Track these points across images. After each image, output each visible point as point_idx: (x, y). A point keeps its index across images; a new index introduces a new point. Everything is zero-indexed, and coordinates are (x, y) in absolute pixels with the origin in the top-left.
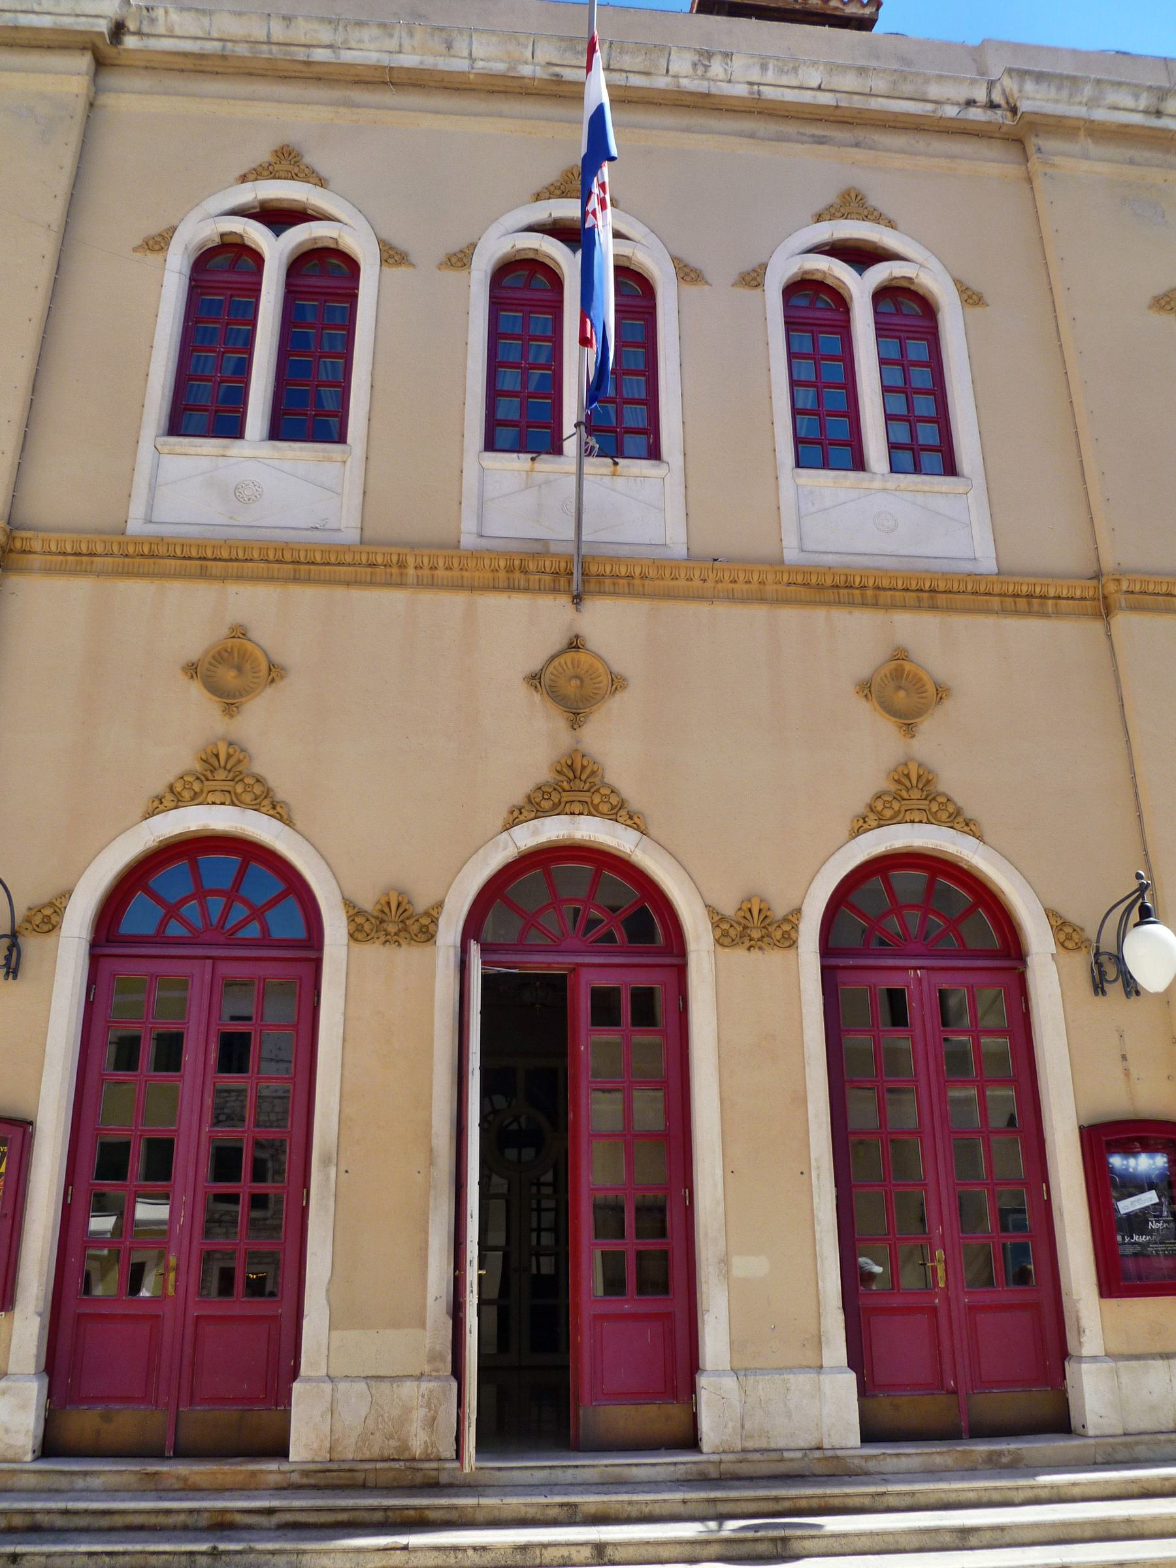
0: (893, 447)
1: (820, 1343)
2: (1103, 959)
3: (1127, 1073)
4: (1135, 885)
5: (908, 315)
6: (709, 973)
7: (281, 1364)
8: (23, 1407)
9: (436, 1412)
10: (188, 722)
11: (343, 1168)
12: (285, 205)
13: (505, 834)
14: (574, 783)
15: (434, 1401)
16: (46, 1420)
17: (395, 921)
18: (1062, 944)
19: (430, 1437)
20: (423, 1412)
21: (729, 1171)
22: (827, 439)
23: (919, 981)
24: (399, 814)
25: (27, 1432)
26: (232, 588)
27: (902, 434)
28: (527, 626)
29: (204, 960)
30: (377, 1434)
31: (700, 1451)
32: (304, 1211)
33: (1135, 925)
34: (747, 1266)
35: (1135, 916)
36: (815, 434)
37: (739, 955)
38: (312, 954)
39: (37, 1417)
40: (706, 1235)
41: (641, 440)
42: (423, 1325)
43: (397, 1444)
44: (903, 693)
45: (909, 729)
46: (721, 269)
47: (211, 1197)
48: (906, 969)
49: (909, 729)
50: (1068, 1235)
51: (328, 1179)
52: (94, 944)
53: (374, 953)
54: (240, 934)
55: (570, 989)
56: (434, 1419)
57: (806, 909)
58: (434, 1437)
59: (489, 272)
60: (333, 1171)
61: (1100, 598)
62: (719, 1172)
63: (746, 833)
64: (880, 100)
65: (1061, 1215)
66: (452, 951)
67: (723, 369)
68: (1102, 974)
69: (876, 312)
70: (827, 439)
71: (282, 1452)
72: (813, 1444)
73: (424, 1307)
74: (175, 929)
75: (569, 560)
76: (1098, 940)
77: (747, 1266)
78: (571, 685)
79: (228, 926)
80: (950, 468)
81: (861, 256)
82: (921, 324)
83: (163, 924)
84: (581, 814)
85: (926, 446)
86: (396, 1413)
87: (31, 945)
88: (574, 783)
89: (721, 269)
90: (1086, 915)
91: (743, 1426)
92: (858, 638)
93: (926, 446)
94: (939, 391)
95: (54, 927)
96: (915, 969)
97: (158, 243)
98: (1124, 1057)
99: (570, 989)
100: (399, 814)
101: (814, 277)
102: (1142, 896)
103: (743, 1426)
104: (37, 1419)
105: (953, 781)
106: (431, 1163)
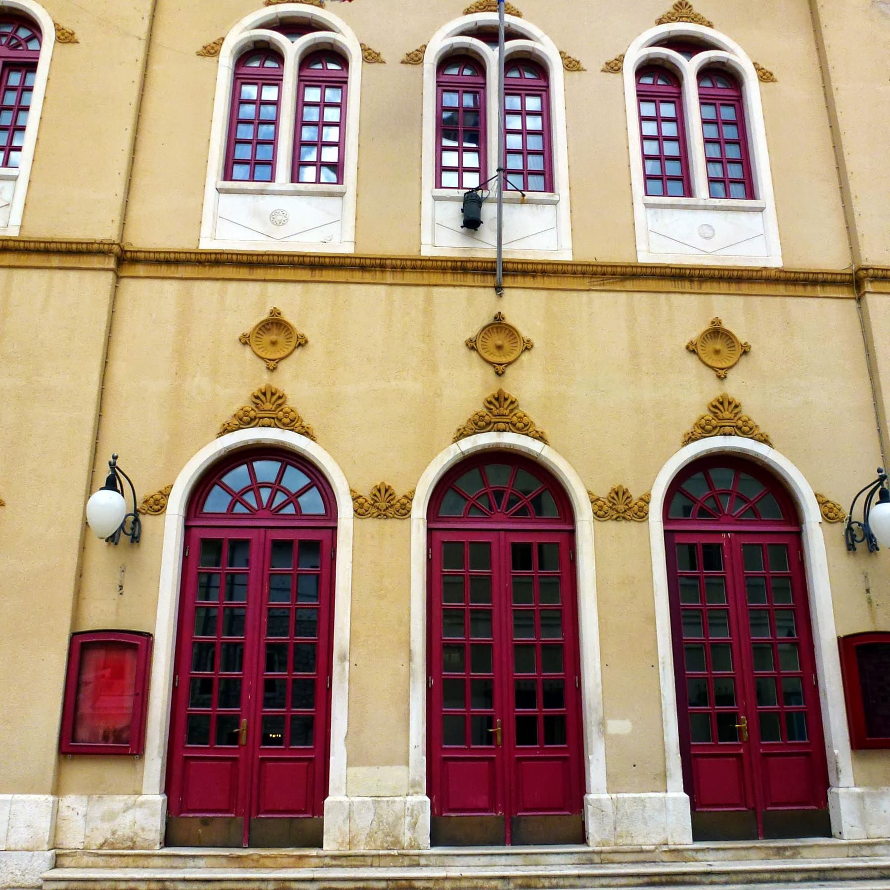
0: (712, 180)
1: (665, 776)
2: (854, 526)
3: (870, 602)
4: (876, 476)
5: (723, 80)
6: (592, 542)
7: (320, 787)
8: (153, 815)
9: (417, 819)
10: (243, 378)
11: (354, 661)
12: (296, 21)
13: (455, 444)
14: (500, 410)
15: (416, 812)
16: (166, 824)
17: (383, 504)
18: (826, 515)
19: (413, 835)
20: (408, 819)
21: (605, 665)
22: (669, 176)
23: (729, 541)
24: (382, 417)
25: (156, 831)
26: (271, 286)
27: (717, 171)
28: (465, 308)
29: (258, 559)
30: (380, 833)
31: (588, 846)
32: (329, 690)
33: (877, 503)
34: (619, 727)
35: (876, 497)
36: (658, 172)
37: (611, 526)
38: (331, 524)
39: (162, 821)
40: (590, 706)
41: (540, 180)
42: (408, 764)
43: (392, 839)
44: (718, 346)
45: (722, 378)
46: (593, 62)
47: (269, 545)
48: (721, 532)
49: (722, 378)
50: (830, 708)
51: (344, 669)
52: (187, 518)
53: (371, 525)
54: (281, 512)
55: (502, 524)
56: (416, 823)
57: (653, 493)
58: (415, 835)
59: (436, 64)
60: (347, 664)
61: (855, 282)
62: (598, 665)
63: (614, 422)
64: (626, 860)
65: (825, 694)
66: (421, 522)
67: (597, 120)
68: (853, 537)
69: (699, 87)
70: (669, 176)
71: (320, 846)
72: (662, 841)
73: (408, 752)
74: (239, 509)
75: (494, 262)
76: (851, 513)
77: (619, 727)
78: (498, 342)
79: (274, 506)
80: (751, 194)
81: (689, 45)
82: (731, 94)
83: (232, 506)
84: (504, 431)
85: (736, 177)
86: (391, 819)
87: (147, 521)
88: (500, 410)
89: (593, 62)
90: (843, 501)
91: (615, 829)
92: (690, 312)
93: (736, 177)
94: (743, 142)
95: (162, 507)
96: (726, 532)
97: (211, 51)
98: (868, 591)
99: (502, 524)
100: (382, 417)
101: (657, 63)
102: (881, 484)
103: (615, 829)
104: (162, 824)
105: (752, 407)
106: (410, 660)
